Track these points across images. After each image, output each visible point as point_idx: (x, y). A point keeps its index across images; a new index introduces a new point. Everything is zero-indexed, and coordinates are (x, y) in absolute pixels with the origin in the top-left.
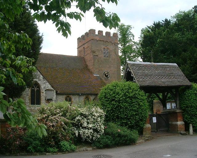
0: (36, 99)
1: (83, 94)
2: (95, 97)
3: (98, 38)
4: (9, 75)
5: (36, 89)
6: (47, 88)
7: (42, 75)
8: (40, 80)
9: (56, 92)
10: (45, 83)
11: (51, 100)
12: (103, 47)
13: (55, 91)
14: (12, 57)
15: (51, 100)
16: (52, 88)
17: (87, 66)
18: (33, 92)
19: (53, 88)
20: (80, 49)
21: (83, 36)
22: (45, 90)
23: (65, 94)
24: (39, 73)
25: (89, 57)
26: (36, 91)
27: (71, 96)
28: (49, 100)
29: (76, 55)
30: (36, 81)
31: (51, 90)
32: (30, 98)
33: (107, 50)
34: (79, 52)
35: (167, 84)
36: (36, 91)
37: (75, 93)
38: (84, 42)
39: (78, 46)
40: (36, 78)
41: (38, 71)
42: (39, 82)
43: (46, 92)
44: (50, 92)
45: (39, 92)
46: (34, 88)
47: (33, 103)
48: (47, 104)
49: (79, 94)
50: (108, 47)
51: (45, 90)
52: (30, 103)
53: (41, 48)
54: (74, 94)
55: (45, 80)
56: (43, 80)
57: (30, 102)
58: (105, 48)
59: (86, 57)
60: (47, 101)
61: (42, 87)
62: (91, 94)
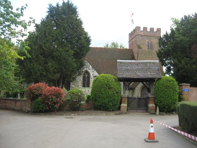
0: (87, 83)
3: (142, 34)
5: (86, 76)
7: (91, 65)
8: (89, 69)
10: (93, 72)
12: (147, 41)
18: (84, 77)
20: (130, 43)
21: (132, 32)
24: (89, 64)
25: (135, 50)
26: (86, 77)
29: (128, 48)
30: (86, 70)
32: (82, 82)
34: (130, 45)
35: (150, 77)
36: (86, 77)
38: (132, 36)
40: (87, 68)
42: (89, 71)
45: (89, 77)
47: (84, 86)
51: (94, 77)
55: (94, 69)
61: (91, 74)
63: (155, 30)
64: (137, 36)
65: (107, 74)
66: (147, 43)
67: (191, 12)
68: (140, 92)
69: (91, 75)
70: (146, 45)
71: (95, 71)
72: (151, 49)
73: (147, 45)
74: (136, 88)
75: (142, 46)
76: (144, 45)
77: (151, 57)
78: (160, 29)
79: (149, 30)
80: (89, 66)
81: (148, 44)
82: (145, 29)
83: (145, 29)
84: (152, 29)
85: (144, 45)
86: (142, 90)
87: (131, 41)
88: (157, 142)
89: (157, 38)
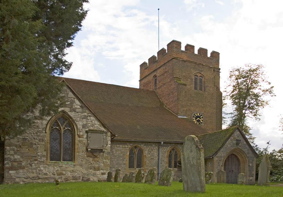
6: (91, 128)
8: (74, 110)
9: (113, 136)
10: (85, 117)
12: (194, 72)
13: (109, 134)
14: (20, 136)
15: (101, 151)
16: (103, 129)
17: (162, 104)
19: (105, 127)
21: (152, 59)
22: (87, 132)
24: (71, 95)
27: (142, 146)
28: (94, 153)
31: (102, 132)
33: (201, 78)
34: (140, 85)
39: (141, 77)
41: (68, 90)
42: (72, 114)
43: (87, 136)
44: (101, 135)
46: (59, 125)
47: (55, 157)
49: (160, 143)
50: (202, 73)
51: (87, 132)
52: (49, 158)
53: (83, 16)
56: (81, 110)
57: (49, 155)
58: (196, 75)
59: (159, 91)
60: (91, 154)
61: (80, 124)
64: (174, 60)
65: (65, 161)
66: (193, 78)
67: (1, 185)
69: (80, 126)
70: (192, 80)
76: (189, 80)
77: (200, 104)
78: (218, 54)
80: (72, 102)
81: (196, 79)
84: (203, 51)
85: (189, 80)
86: (228, 157)
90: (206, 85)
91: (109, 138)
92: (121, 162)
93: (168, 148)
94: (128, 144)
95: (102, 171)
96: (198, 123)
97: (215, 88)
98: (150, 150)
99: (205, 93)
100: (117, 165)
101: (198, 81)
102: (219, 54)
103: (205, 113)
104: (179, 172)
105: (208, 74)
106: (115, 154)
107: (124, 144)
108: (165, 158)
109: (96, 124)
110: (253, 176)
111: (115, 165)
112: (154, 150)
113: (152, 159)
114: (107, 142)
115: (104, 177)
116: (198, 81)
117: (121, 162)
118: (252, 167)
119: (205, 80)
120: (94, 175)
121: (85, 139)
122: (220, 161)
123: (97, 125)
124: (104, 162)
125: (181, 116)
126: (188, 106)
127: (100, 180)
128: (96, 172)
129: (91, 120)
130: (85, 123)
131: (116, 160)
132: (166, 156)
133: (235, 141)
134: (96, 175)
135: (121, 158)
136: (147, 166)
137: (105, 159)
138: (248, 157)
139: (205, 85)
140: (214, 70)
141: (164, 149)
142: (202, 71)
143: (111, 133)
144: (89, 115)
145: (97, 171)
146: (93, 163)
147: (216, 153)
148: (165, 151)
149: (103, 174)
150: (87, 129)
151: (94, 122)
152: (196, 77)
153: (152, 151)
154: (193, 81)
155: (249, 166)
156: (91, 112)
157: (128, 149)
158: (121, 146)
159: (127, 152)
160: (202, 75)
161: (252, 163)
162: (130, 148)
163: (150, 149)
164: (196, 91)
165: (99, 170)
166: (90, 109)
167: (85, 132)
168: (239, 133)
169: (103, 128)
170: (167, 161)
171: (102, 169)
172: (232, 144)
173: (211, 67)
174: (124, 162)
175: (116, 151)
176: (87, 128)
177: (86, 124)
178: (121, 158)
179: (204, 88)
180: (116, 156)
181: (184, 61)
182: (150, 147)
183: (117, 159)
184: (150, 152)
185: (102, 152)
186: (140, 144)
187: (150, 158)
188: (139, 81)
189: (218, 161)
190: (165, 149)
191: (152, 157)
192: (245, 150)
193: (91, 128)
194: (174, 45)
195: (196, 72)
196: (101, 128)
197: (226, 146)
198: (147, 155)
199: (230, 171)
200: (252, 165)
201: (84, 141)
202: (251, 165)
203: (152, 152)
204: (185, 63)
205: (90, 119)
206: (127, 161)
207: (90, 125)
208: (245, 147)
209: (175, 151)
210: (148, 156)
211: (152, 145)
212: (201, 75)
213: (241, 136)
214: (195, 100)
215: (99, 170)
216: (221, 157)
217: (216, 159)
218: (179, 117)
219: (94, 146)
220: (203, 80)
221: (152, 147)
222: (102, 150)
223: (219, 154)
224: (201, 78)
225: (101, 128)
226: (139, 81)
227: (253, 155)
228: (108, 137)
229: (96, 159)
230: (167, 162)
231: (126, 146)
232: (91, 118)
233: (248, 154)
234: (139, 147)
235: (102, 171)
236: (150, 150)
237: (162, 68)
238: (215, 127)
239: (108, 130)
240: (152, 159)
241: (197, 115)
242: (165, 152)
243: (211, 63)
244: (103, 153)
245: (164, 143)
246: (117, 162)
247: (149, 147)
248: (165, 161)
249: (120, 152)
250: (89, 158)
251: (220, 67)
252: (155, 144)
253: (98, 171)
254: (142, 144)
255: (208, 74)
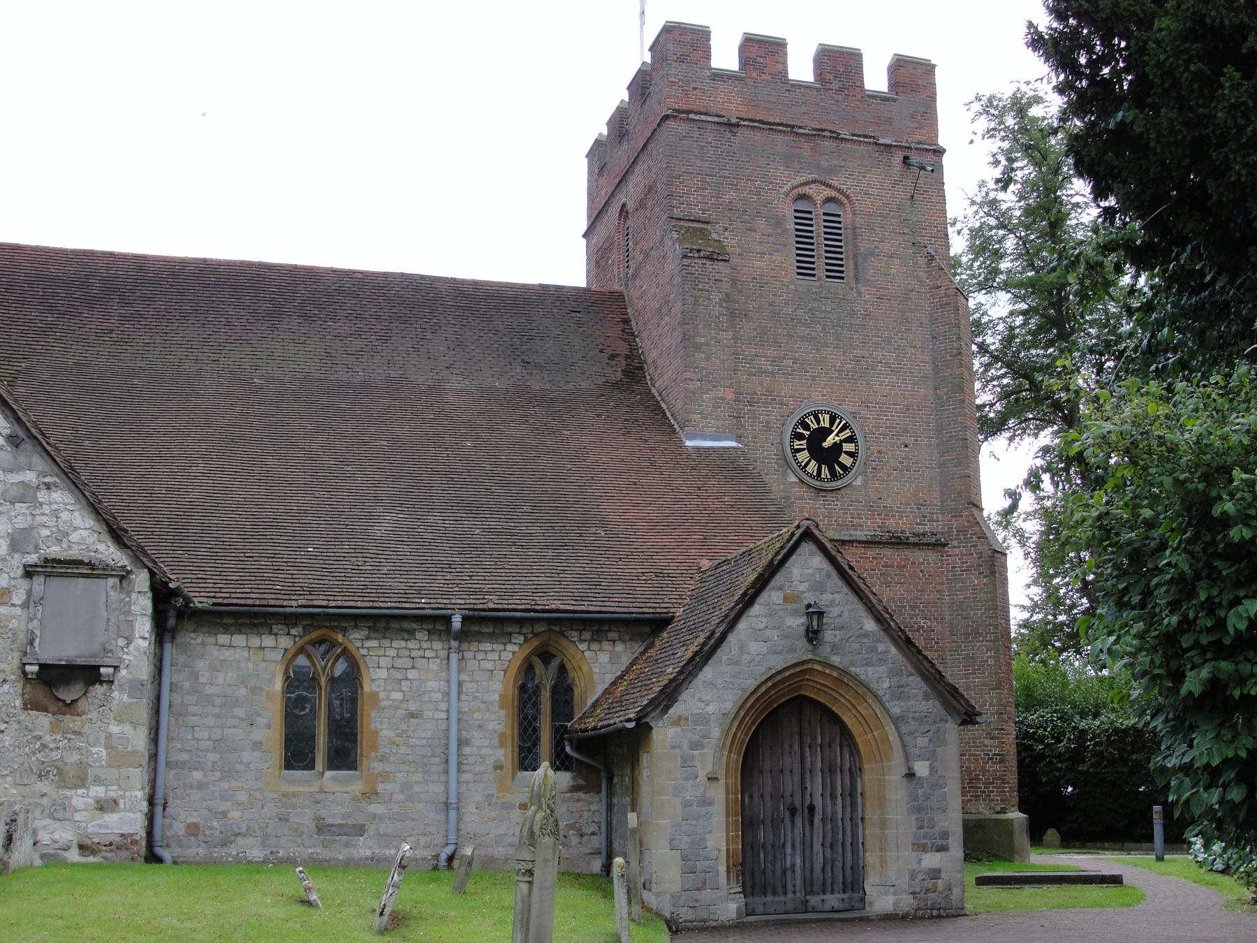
1: (484, 624)
2: (638, 648)
3: (732, 105)
4: (624, 718)
6: (55, 551)
9: (163, 595)
11: (89, 674)
13: (141, 580)
15: (89, 674)
19: (117, 536)
20: (602, 232)
23: (290, 619)
25: (654, 290)
27: (356, 640)
29: (581, 282)
31: (88, 569)
33: (831, 208)
34: (598, 260)
37: (409, 607)
48: (43, 721)
49: (447, 619)
50: (834, 183)
51: (29, 573)
54: (384, 623)
55: (39, 461)
59: (633, 293)
60: (40, 694)
62: (599, 626)
63: (876, 79)
64: (671, 124)
66: (787, 210)
68: (718, 793)
71: (61, 497)
72: (835, 273)
73: (791, 226)
74: (664, 734)
75: (730, 241)
76: (761, 224)
78: (927, 69)
79: (801, 69)
81: (803, 218)
82: (762, 52)
83: (762, 52)
84: (839, 65)
85: (761, 224)
87: (614, 210)
88: (513, 775)
89: (898, 158)
90: (864, 246)
91: (143, 604)
92: (239, 734)
93: (510, 647)
94: (275, 631)
95: (98, 791)
96: (825, 472)
97: (922, 261)
98: (399, 663)
99: (860, 294)
100: (214, 750)
101: (818, 228)
102: (934, 66)
103: (864, 412)
104: (581, 795)
105: (868, 186)
106: (209, 690)
107: (255, 626)
108: (488, 710)
109: (76, 529)
110: (942, 849)
111: (207, 751)
112: (421, 663)
113: (412, 715)
114: (131, 624)
115: (107, 827)
116: (818, 228)
117: (239, 734)
118: (937, 782)
119: (859, 221)
120: (59, 812)
121: (18, 611)
122: (695, 745)
123: (82, 535)
124: (109, 736)
125: (704, 438)
126: (761, 372)
127: (88, 842)
128: (68, 793)
129: (54, 507)
130: (21, 523)
131: (211, 721)
132: (497, 697)
133: (795, 613)
134: (68, 815)
135: (241, 713)
136: (383, 759)
137: (120, 721)
138: (897, 721)
139: (855, 246)
140: (906, 158)
141: (480, 656)
142: (832, 171)
143: (152, 573)
144: (47, 480)
145: (75, 787)
146: (52, 745)
147: (669, 695)
148: (489, 666)
149: (104, 806)
150: (33, 558)
151: (65, 516)
152: (803, 206)
153: (413, 667)
154: (785, 231)
155: (910, 775)
156: (54, 467)
157: (278, 656)
158: (239, 640)
159: (273, 674)
160: (839, 190)
161: (931, 756)
162: (286, 650)
163: (398, 656)
164: (805, 282)
165: (83, 786)
166: (49, 448)
167: (20, 572)
168: (826, 566)
169: (112, 549)
170: (501, 728)
171: (98, 781)
172: (774, 635)
173: (887, 141)
174: (257, 735)
175: (213, 668)
176: (31, 548)
177: (27, 532)
178: (241, 713)
179: (851, 262)
180: (209, 700)
181: (729, 125)
182: (403, 644)
183: (217, 717)
184: (399, 676)
185: (101, 682)
186: (344, 630)
187: (401, 712)
188: (585, 236)
189: (685, 745)
190: (490, 656)
191: (413, 707)
192: (869, 674)
193: (54, 548)
194: (681, 45)
195: (799, 180)
196: (101, 547)
197: (735, 651)
198: (382, 695)
199: (793, 811)
200: (933, 770)
201: (14, 624)
202: (922, 769)
203: (412, 674)
204: (734, 134)
205: (50, 503)
206: (269, 726)
207: (45, 532)
208: (874, 650)
209: (555, 664)
210: (388, 699)
211: (411, 633)
212: (834, 194)
213: (836, 581)
214: (803, 338)
215: (82, 782)
216: (703, 719)
217: (672, 731)
218: (689, 443)
219: (62, 649)
220: (846, 218)
221: (411, 644)
222: (99, 667)
223: (689, 702)
224: (831, 208)
225: (101, 547)
226: (585, 236)
227: (933, 707)
228: (134, 596)
229: (72, 722)
230: (502, 735)
231: (268, 641)
232: (57, 495)
233: (899, 693)
234: (341, 644)
235: (98, 791)
236: (399, 663)
237: (638, 169)
238: (936, 494)
239: (136, 559)
240: (412, 715)
241: (814, 426)
242: (492, 669)
243: (888, 121)
244: (105, 686)
245: (464, 618)
246: (217, 734)
247: (395, 644)
248: (490, 726)
249: (232, 676)
250: (33, 713)
251: (942, 142)
252: (431, 627)
253: (80, 791)
254: (356, 627)
255: (868, 186)
